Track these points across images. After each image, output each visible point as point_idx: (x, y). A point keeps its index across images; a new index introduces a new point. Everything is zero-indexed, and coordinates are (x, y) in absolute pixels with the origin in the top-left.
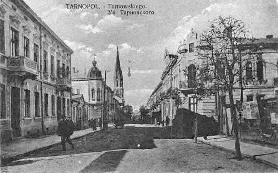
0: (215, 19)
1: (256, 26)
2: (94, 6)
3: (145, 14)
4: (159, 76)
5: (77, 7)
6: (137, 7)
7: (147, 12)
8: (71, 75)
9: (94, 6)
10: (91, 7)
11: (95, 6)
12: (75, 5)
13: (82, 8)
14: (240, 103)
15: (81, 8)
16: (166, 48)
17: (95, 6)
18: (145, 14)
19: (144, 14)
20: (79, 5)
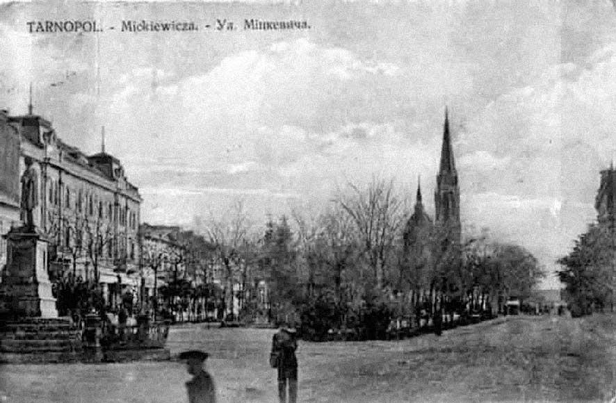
0: (222, 22)
1: (533, 212)
2: (90, 24)
3: (271, 28)
4: (209, 153)
5: (53, 28)
6: (277, 26)
7: (69, 25)
8: (33, 184)
9: (90, 24)
10: (84, 28)
11: (93, 25)
12: (47, 22)
13: (63, 29)
14: (429, 314)
15: (61, 30)
16: (309, 27)
17: (93, 25)
18: (271, 28)
19: (270, 30)
20: (56, 24)
